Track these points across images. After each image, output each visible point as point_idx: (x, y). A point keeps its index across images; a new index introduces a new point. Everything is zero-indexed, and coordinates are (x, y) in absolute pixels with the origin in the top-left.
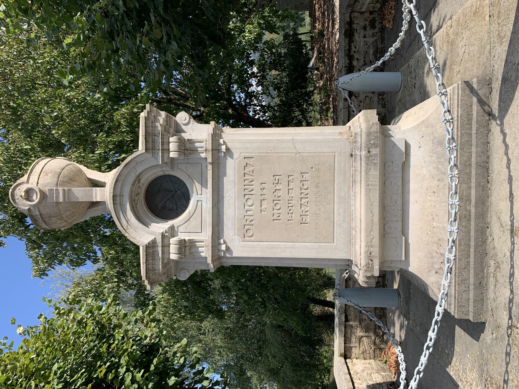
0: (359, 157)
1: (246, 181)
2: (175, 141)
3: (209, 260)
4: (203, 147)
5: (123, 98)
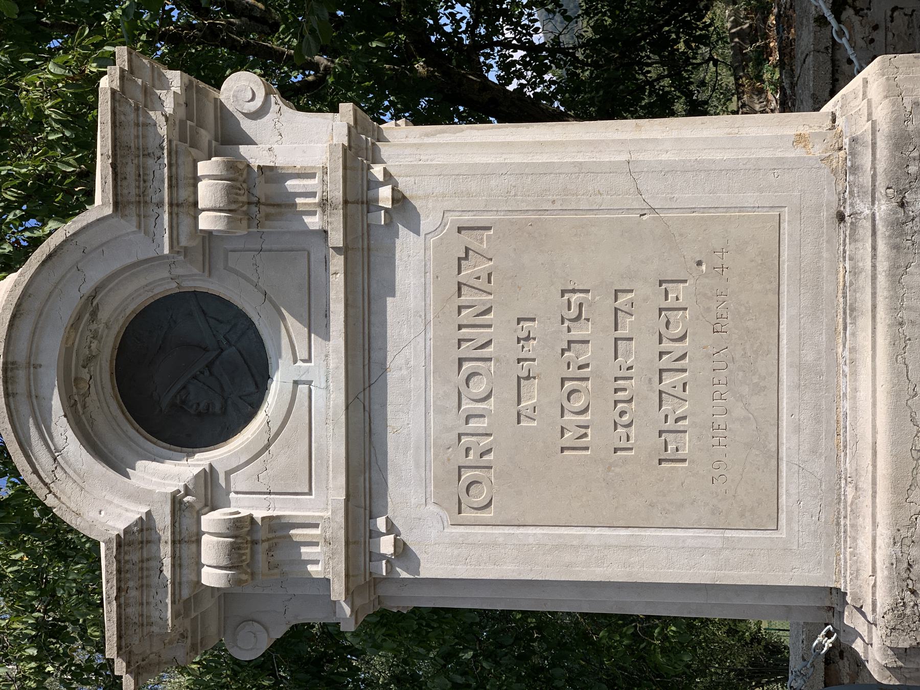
0: (868, 224)
1: (464, 312)
2: (216, 172)
3: (338, 591)
4: (313, 195)
5: (52, 26)
